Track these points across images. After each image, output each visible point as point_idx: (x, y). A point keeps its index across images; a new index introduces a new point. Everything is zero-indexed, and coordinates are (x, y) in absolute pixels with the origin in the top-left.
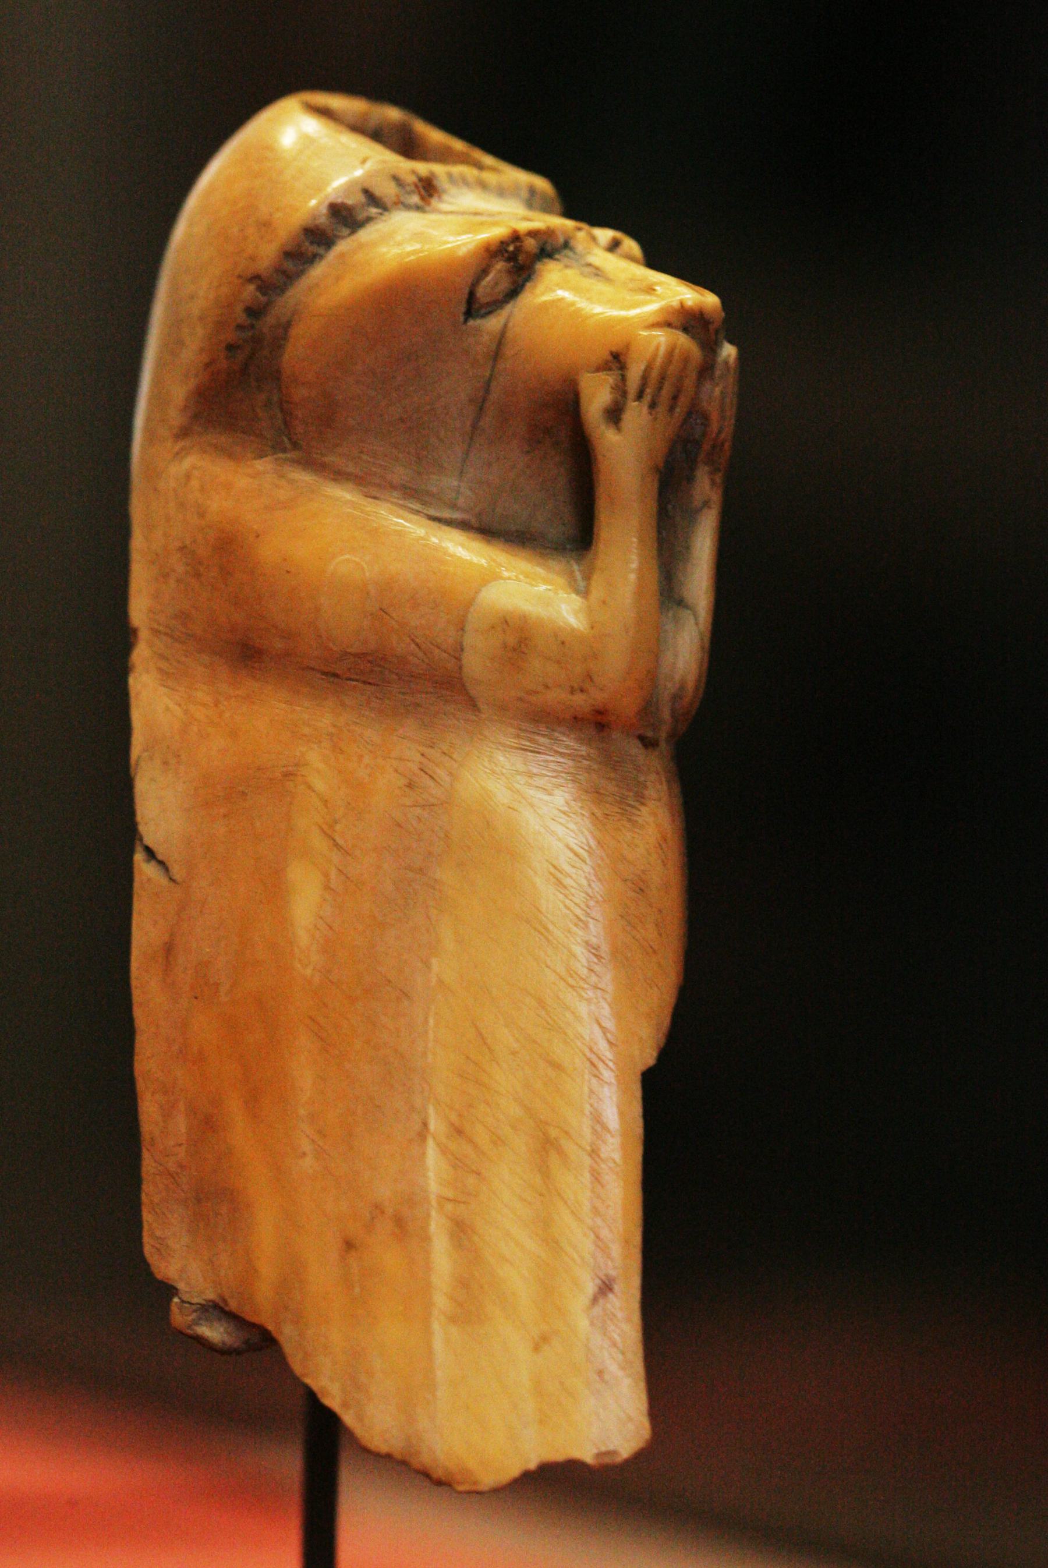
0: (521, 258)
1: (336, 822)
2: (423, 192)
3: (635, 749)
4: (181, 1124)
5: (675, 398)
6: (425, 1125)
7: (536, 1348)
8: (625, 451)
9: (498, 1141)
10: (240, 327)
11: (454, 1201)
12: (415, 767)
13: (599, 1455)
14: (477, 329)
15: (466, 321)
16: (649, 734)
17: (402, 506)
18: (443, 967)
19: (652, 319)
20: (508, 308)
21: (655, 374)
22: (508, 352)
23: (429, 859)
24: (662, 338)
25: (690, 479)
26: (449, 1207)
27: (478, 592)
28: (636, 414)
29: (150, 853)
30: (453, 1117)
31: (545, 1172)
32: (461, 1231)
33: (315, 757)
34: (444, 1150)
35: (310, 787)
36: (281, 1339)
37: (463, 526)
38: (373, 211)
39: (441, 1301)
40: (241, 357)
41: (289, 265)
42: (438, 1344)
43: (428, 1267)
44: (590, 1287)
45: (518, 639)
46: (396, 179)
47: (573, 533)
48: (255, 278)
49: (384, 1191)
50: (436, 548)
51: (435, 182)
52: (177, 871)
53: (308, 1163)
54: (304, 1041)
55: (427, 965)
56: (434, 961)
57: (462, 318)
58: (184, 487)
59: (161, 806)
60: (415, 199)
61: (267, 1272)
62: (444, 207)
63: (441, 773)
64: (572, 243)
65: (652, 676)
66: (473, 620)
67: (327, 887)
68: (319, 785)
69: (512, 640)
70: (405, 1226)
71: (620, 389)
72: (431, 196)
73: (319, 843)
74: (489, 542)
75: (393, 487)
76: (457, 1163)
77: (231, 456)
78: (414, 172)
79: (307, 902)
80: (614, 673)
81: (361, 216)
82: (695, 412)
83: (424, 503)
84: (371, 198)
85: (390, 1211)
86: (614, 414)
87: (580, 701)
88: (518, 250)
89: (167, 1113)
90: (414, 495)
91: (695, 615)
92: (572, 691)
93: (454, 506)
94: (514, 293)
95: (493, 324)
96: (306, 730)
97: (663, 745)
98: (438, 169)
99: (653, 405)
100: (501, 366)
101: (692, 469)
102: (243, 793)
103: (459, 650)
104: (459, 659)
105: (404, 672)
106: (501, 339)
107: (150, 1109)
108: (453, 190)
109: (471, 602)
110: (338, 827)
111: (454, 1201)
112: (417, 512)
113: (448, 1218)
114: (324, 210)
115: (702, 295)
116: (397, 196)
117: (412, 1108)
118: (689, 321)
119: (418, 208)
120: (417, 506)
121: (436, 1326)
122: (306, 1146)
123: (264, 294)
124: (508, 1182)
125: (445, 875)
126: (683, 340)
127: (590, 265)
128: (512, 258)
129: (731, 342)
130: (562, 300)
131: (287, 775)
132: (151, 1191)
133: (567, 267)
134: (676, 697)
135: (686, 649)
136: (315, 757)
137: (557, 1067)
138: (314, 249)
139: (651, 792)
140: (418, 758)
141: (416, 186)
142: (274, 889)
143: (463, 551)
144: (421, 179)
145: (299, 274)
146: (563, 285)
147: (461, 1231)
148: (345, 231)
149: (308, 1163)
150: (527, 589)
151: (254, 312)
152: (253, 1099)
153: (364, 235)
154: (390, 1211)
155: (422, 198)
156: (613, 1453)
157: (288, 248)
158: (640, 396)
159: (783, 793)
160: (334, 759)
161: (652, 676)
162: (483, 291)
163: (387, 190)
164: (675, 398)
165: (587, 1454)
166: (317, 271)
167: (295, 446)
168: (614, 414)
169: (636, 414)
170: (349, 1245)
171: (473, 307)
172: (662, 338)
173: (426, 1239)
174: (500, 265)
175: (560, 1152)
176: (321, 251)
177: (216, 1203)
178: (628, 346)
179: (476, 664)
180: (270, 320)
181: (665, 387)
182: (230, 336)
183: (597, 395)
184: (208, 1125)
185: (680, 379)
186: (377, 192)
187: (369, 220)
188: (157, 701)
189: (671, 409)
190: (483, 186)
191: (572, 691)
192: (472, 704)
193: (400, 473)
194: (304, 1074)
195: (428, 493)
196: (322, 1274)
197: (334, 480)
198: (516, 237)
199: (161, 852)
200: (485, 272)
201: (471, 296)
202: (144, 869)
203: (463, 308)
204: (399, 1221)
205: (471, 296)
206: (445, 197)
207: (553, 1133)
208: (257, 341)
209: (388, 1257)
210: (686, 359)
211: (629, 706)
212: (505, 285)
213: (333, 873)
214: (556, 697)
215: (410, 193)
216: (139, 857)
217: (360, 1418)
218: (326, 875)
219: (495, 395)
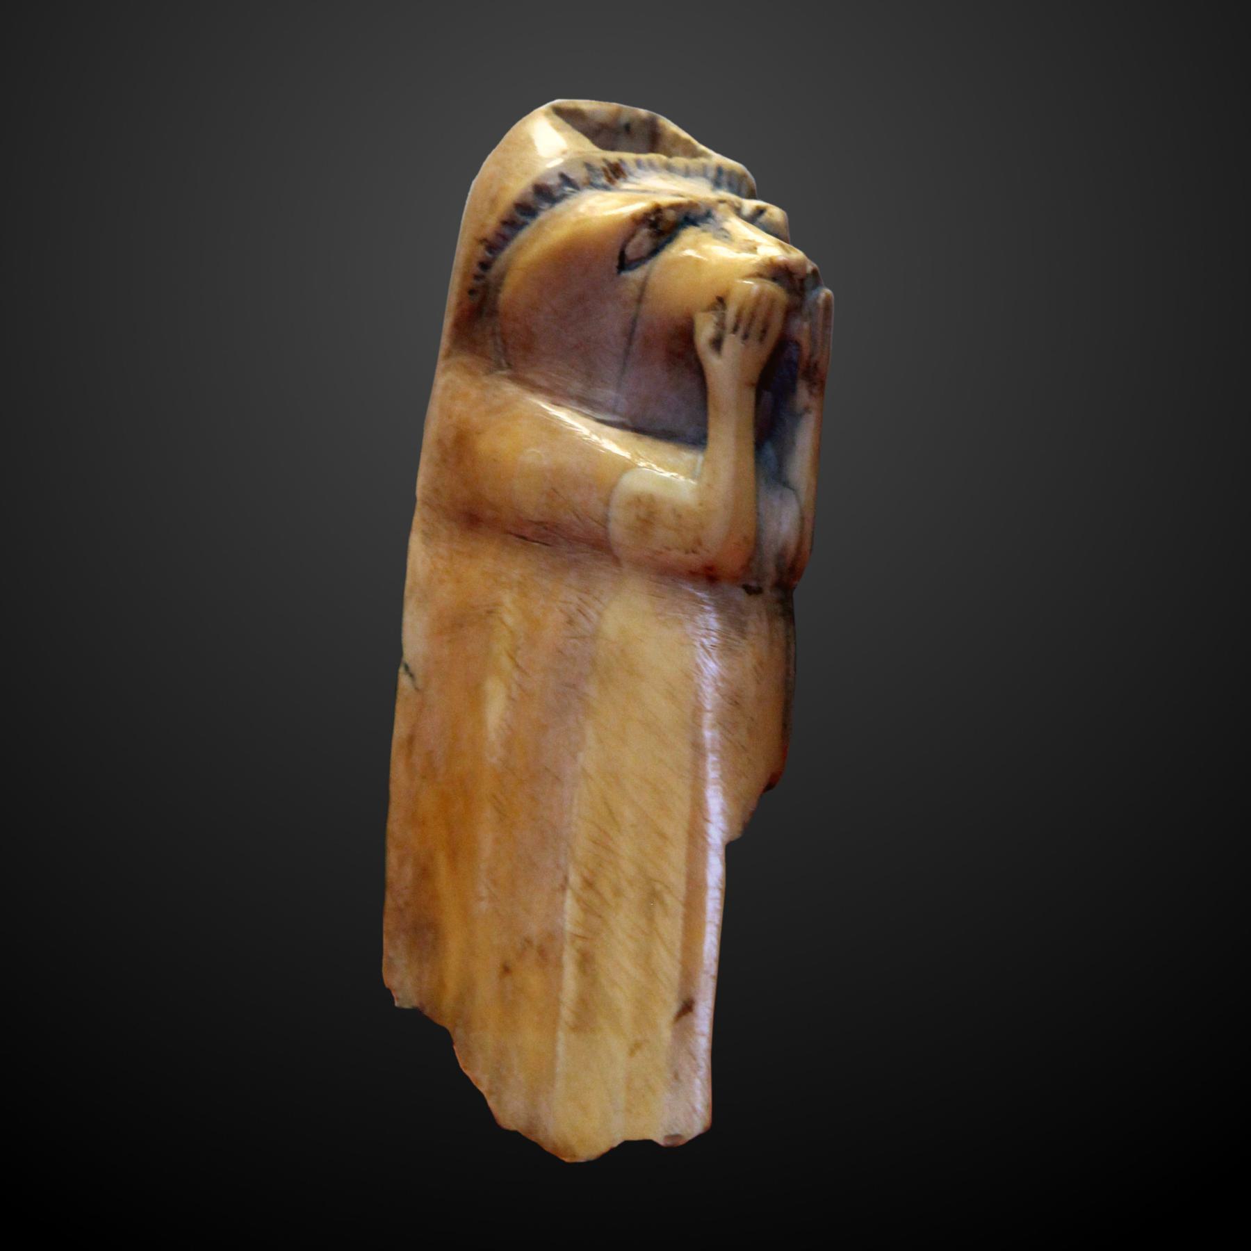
0: (661, 226)
1: (519, 648)
2: (611, 175)
3: (740, 596)
4: (409, 872)
5: (764, 332)
6: (566, 879)
7: (632, 1053)
8: (727, 369)
9: (618, 892)
10: (477, 277)
11: (583, 938)
12: (573, 608)
13: (668, 1137)
14: (625, 279)
15: (619, 273)
16: (753, 584)
17: (578, 412)
18: (589, 759)
19: (749, 270)
20: (647, 267)
21: (746, 313)
22: (648, 296)
23: (573, 681)
24: (753, 286)
25: (793, 391)
26: (579, 943)
27: (620, 476)
28: (732, 344)
29: (407, 668)
30: (586, 874)
31: (651, 920)
32: (586, 961)
33: (508, 599)
34: (579, 899)
35: (503, 623)
37: (621, 426)
38: (568, 189)
39: (566, 1014)
40: (477, 298)
41: (506, 231)
42: (561, 1049)
43: (560, 989)
44: (675, 1008)
45: (648, 512)
46: (588, 166)
47: (687, 432)
48: (483, 241)
49: (534, 929)
50: (594, 444)
51: (623, 167)
52: (420, 682)
53: (484, 906)
54: (488, 813)
55: (575, 757)
56: (581, 756)
57: (615, 271)
58: (457, 393)
59: (416, 633)
60: (604, 180)
61: (452, 986)
62: (626, 186)
63: (591, 613)
64: (714, 212)
65: (756, 542)
66: (618, 498)
67: (510, 698)
68: (509, 620)
69: (642, 514)
70: (545, 953)
71: (721, 325)
72: (618, 177)
73: (505, 662)
74: (639, 439)
75: (572, 397)
76: (587, 908)
77: (471, 373)
78: (605, 160)
79: (496, 710)
80: (717, 537)
81: (557, 194)
83: (594, 409)
84: (565, 179)
85: (536, 943)
86: (717, 343)
87: (695, 560)
88: (658, 219)
89: (402, 862)
90: (584, 403)
91: (797, 496)
92: (687, 552)
93: (614, 412)
94: (655, 251)
95: (636, 275)
96: (503, 579)
97: (767, 591)
98: (628, 157)
99: (745, 337)
100: (644, 306)
101: (794, 382)
102: (462, 623)
103: (604, 521)
104: (605, 527)
105: (566, 534)
106: (643, 286)
108: (640, 172)
109: (612, 487)
110: (519, 652)
111: (583, 938)
112: (586, 416)
113: (578, 951)
114: (530, 190)
115: (788, 252)
116: (588, 178)
117: (558, 867)
118: (779, 273)
119: (606, 188)
120: (588, 412)
121: (561, 1035)
122: (484, 892)
123: (490, 252)
124: (623, 921)
125: (592, 689)
126: (771, 287)
127: (723, 229)
128: (653, 225)
130: (690, 257)
131: (490, 612)
133: (704, 231)
136: (508, 599)
137: (663, 836)
138: (522, 218)
139: (751, 628)
140: (576, 600)
141: (605, 170)
142: (475, 696)
143: (612, 444)
144: (610, 165)
145: (514, 235)
146: (694, 246)
147: (586, 961)
148: (546, 205)
149: (484, 906)
150: (663, 475)
151: (485, 265)
152: (453, 856)
153: (559, 208)
154: (536, 943)
155: (610, 180)
157: (506, 218)
158: (735, 330)
160: (520, 598)
161: (756, 542)
162: (630, 252)
163: (578, 174)
164: (764, 332)
165: (659, 1137)
166: (524, 234)
167: (509, 366)
168: (717, 343)
169: (732, 344)
170: (506, 970)
171: (624, 263)
172: (753, 286)
173: (559, 965)
174: (645, 231)
175: (663, 903)
176: (528, 220)
177: (426, 935)
178: (728, 291)
179: (618, 531)
180: (494, 271)
183: (705, 331)
184: (425, 873)
185: (769, 313)
186: (572, 176)
187: (564, 196)
188: (421, 556)
189: (761, 340)
190: (669, 168)
191: (687, 552)
192: (617, 561)
193: (576, 387)
194: (487, 839)
195: (595, 402)
196: (486, 988)
197: (532, 392)
198: (658, 210)
199: (411, 665)
200: (633, 236)
201: (622, 255)
202: (404, 680)
203: (616, 263)
204: (542, 952)
205: (622, 255)
206: (630, 178)
207: (658, 887)
208: (486, 287)
209: (533, 981)
210: (773, 301)
211: (732, 562)
212: (647, 246)
213: (514, 687)
214: (676, 555)
215: (598, 176)
216: (402, 670)
218: (509, 688)
219: (638, 329)
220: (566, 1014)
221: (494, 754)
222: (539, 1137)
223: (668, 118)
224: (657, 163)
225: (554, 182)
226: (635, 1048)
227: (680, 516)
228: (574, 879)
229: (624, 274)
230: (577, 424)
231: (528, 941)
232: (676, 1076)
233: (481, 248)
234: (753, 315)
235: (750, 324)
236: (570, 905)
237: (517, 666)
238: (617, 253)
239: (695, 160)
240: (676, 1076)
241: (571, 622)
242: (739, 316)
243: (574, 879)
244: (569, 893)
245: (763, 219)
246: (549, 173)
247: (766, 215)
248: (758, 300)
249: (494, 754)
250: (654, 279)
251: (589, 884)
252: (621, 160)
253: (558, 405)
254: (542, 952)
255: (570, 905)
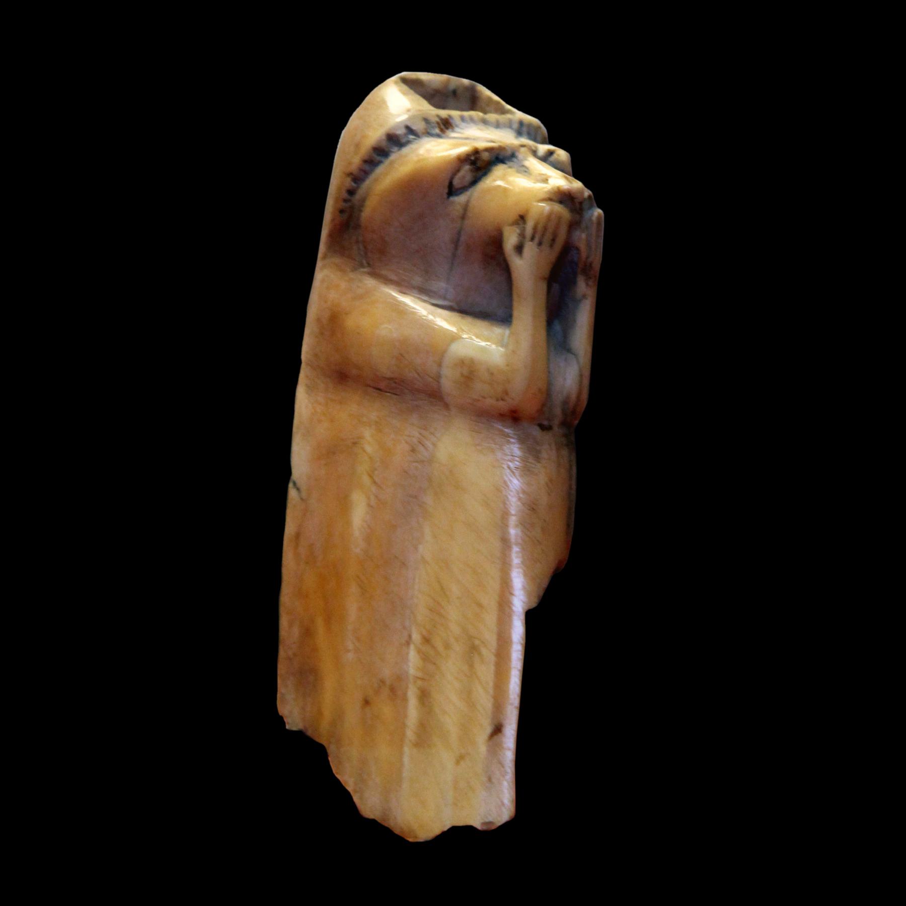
0: (479, 164)
1: (376, 469)
2: (442, 127)
3: (536, 431)
4: (296, 631)
5: (553, 240)
6: (410, 636)
7: (458, 762)
8: (526, 267)
9: (447, 646)
10: (345, 201)
11: (422, 679)
12: (415, 440)
13: (484, 824)
14: (453, 202)
15: (448, 197)
16: (546, 423)
17: (419, 298)
18: (426, 549)
19: (543, 196)
20: (468, 193)
21: (540, 227)
22: (469, 214)
23: (415, 493)
24: (546, 207)
25: (574, 283)
26: (419, 683)
27: (449, 345)
28: (530, 249)
29: (295, 484)
30: (424, 633)
31: (471, 666)
32: (424, 696)
33: (368, 434)
34: (419, 651)
35: (364, 451)
36: (329, 751)
37: (450, 308)
38: (411, 137)
39: (410, 734)
40: (345, 216)
41: (367, 167)
42: (406, 760)
43: (406, 716)
44: (489, 730)
45: (469, 371)
46: (426, 120)
47: (498, 313)
48: (350, 174)
49: (387, 672)
50: (430, 321)
51: (451, 121)
52: (304, 494)
53: (350, 656)
54: (354, 589)
55: (416, 548)
56: (421, 548)
57: (445, 196)
60: (437, 131)
61: (327, 714)
62: (453, 135)
63: (428, 444)
64: (517, 154)
65: (548, 393)
66: (448, 361)
67: (369, 505)
68: (369, 449)
69: (465, 372)
70: (394, 690)
71: (522, 235)
72: (447, 128)
73: (366, 480)
74: (463, 318)
75: (414, 288)
76: (425, 658)
77: (341, 270)
78: (438, 116)
79: (359, 514)
80: (519, 389)
81: (404, 140)
82: (568, 248)
83: (430, 296)
84: (409, 130)
85: (388, 683)
86: (519, 249)
87: (503, 406)
88: (477, 159)
89: (291, 625)
90: (423, 292)
91: (577, 359)
92: (497, 400)
93: (445, 298)
94: (475, 182)
95: (461, 199)
96: (365, 419)
97: (556, 428)
98: (455, 114)
99: (540, 244)
100: (466, 222)
101: (575, 277)
102: (334, 451)
103: (438, 378)
104: (438, 382)
105: (410, 386)
106: (466, 207)
107: (284, 621)
108: (463, 125)
109: (443, 353)
110: (376, 472)
111: (422, 679)
112: (425, 301)
113: (419, 689)
114: (384, 138)
116: (426, 129)
117: (404, 628)
118: (564, 198)
119: (439, 136)
120: (426, 298)
121: (406, 749)
122: (351, 646)
123: (355, 182)
124: (451, 667)
125: (429, 499)
126: (558, 208)
127: (523, 166)
128: (473, 163)
129: (599, 207)
130: (500, 186)
131: (355, 443)
132: (282, 668)
133: (510, 167)
134: (565, 402)
135: (572, 376)
136: (368, 434)
137: (480, 605)
138: (378, 158)
139: (544, 455)
140: (417, 434)
141: (438, 123)
142: (344, 504)
143: (444, 321)
144: (442, 119)
145: (372, 171)
146: (503, 178)
147: (424, 696)
148: (396, 149)
149: (350, 656)
150: (480, 344)
151: (351, 192)
152: (328, 620)
153: (405, 150)
154: (388, 683)
155: (442, 130)
156: (491, 823)
157: (366, 158)
158: (532, 239)
159: (619, 457)
161: (548, 393)
162: (456, 182)
163: (419, 126)
164: (553, 240)
165: (477, 824)
166: (380, 170)
167: (369, 265)
168: (519, 249)
169: (530, 249)
170: (367, 702)
171: (452, 191)
172: (546, 207)
173: (405, 699)
174: (467, 167)
175: (480, 654)
176: (383, 159)
177: (309, 677)
178: (527, 211)
179: (447, 384)
180: (357, 197)
181: (544, 233)
183: (511, 240)
184: (308, 632)
185: (557, 227)
186: (414, 128)
187: (409, 142)
188: (306, 402)
189: (551, 246)
190: (485, 122)
191: (497, 400)
192: (447, 406)
193: (417, 280)
194: (352, 608)
195: (431, 291)
196: (352, 716)
197: (386, 284)
198: (476, 152)
200: (458, 171)
201: (451, 185)
203: (446, 191)
204: (393, 690)
205: (451, 185)
206: (457, 129)
207: (477, 642)
208: (352, 208)
209: (386, 710)
210: (560, 218)
211: (530, 407)
212: (469, 178)
213: (372, 497)
214: (489, 402)
215: (433, 127)
216: (291, 485)
217: (361, 798)
218: (369, 498)
219: (462, 239)
220: (410, 734)
221: (358, 546)
222: (391, 824)
223: (484, 85)
224: (476, 118)
225: (401, 131)
226: (460, 759)
227: (492, 374)
228: (416, 637)
229: (452, 199)
230: (418, 307)
231: (383, 682)
232: (490, 779)
233: (349, 180)
234: (545, 228)
235: (543, 235)
236: (413, 655)
237: (375, 482)
238: (447, 183)
239: (503, 116)
240: (490, 779)
241: (413, 450)
242: (535, 229)
243: (416, 637)
244: (412, 647)
246: (397, 126)
248: (549, 217)
249: (358, 546)
250: (473, 202)
251: (427, 640)
252: (450, 116)
253: (404, 293)
254: (393, 690)
255: (413, 655)
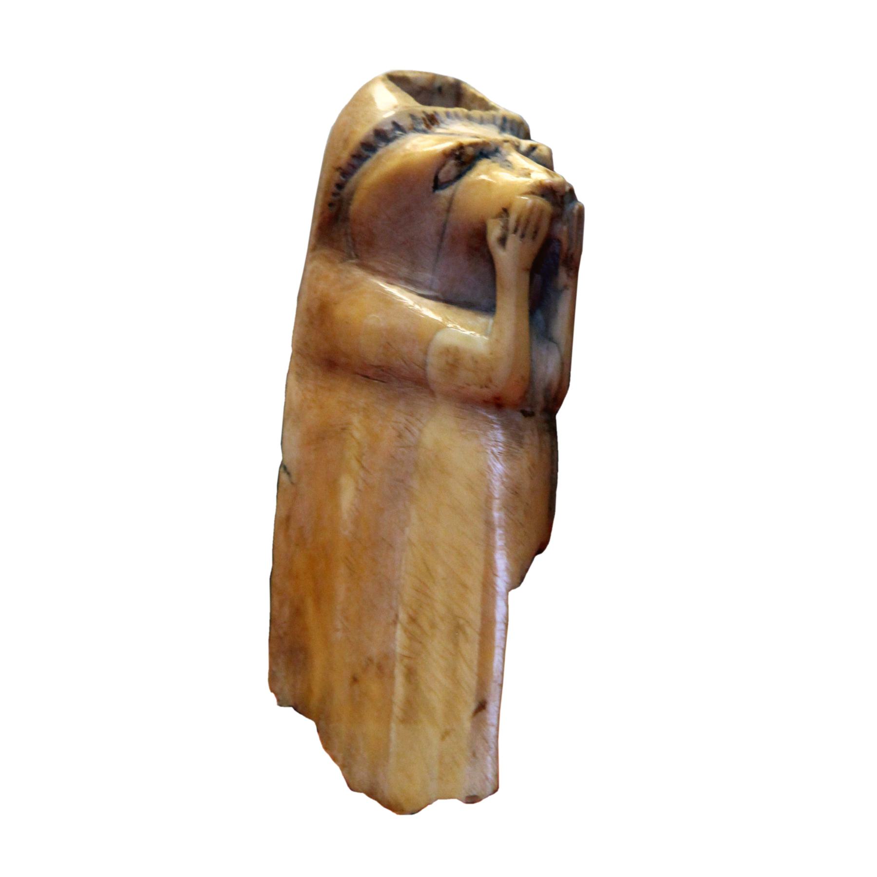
0: (464, 159)
1: (364, 454)
2: (428, 123)
3: (519, 418)
5: (536, 232)
6: (397, 616)
7: (443, 738)
9: (433, 626)
10: (334, 194)
11: (409, 657)
12: (402, 426)
14: (438, 196)
15: (434, 191)
16: (528, 409)
17: (405, 289)
18: (413, 532)
19: (525, 190)
20: (453, 187)
21: (523, 220)
22: (454, 207)
24: (528, 200)
25: (556, 274)
26: (406, 661)
27: (434, 334)
28: (513, 241)
30: (411, 612)
31: (456, 645)
32: (411, 674)
33: (356, 420)
34: (406, 630)
35: (353, 436)
37: (435, 299)
38: (398, 132)
39: (397, 711)
40: (334, 209)
41: (355, 162)
42: (393, 735)
43: (393, 693)
44: (473, 706)
45: (454, 359)
46: (412, 116)
47: (482, 303)
48: (339, 169)
49: (374, 651)
50: (416, 311)
51: (437, 117)
52: (294, 478)
53: (339, 635)
54: (342, 570)
55: (403, 531)
56: (407, 530)
57: (431, 190)
60: (423, 127)
61: (317, 691)
62: (439, 130)
63: (415, 430)
64: (500, 149)
66: (433, 349)
67: (357, 489)
68: (357, 435)
69: (450, 360)
70: (382, 668)
71: (505, 228)
72: (433, 124)
73: (354, 464)
75: (401, 278)
76: (411, 637)
77: (330, 261)
78: (424, 112)
79: (348, 498)
81: (391, 136)
83: (416, 287)
84: (396, 126)
85: (376, 661)
86: (503, 241)
87: (487, 393)
88: (461, 154)
90: (410, 282)
91: (559, 348)
92: (481, 387)
93: (430, 289)
94: (459, 176)
95: (446, 193)
96: (353, 406)
97: (538, 415)
98: (440, 110)
99: (523, 236)
100: (451, 215)
101: (557, 268)
103: (424, 366)
104: (424, 370)
106: (451, 201)
108: (448, 121)
109: (429, 342)
110: (364, 457)
111: (409, 657)
112: (411, 291)
113: (405, 667)
114: (372, 133)
116: (412, 125)
117: (391, 607)
119: (425, 132)
120: (412, 289)
121: (393, 725)
122: (339, 626)
123: (344, 177)
124: (437, 646)
125: (415, 483)
126: (540, 201)
127: (507, 161)
128: (458, 158)
130: (484, 180)
131: (343, 429)
133: (494, 162)
136: (356, 420)
137: (465, 586)
138: (366, 153)
139: (527, 440)
140: (404, 421)
141: (424, 119)
142: (333, 488)
143: (429, 311)
144: (427, 115)
145: (360, 165)
146: (487, 172)
147: (411, 674)
148: (383, 144)
149: (339, 635)
151: (340, 186)
152: (318, 600)
153: (392, 145)
154: (376, 661)
155: (428, 126)
157: (354, 153)
158: (515, 231)
161: (530, 380)
162: (442, 176)
163: (405, 122)
164: (536, 232)
166: (367, 164)
167: (357, 256)
168: (503, 241)
169: (513, 241)
170: (355, 680)
171: (437, 185)
172: (528, 200)
173: (392, 677)
174: (452, 162)
175: (464, 633)
176: (370, 154)
178: (510, 204)
179: (433, 372)
180: (346, 190)
182: (331, 198)
183: (494, 232)
185: (539, 219)
186: (401, 124)
187: (396, 138)
189: (534, 238)
190: (469, 118)
191: (481, 387)
192: (432, 393)
193: (404, 271)
194: (341, 588)
195: (417, 282)
197: (373, 275)
198: (461, 147)
200: (443, 165)
201: (436, 179)
203: (432, 184)
204: (380, 667)
205: (436, 179)
206: (442, 125)
207: (462, 622)
208: (341, 201)
209: (374, 687)
210: (542, 211)
211: (513, 394)
212: (454, 172)
213: (360, 482)
214: (474, 389)
215: (419, 123)
218: (357, 482)
219: (448, 231)
220: (397, 711)
221: (346, 529)
224: (461, 114)
226: (445, 735)
227: (476, 362)
228: (403, 616)
229: (437, 192)
230: (404, 297)
231: (370, 660)
232: (474, 755)
233: (338, 174)
234: (528, 221)
235: (526, 227)
236: (399, 634)
237: (363, 467)
238: (432, 178)
240: (474, 755)
241: (400, 436)
242: (518, 222)
243: (403, 616)
244: (399, 626)
245: (535, 153)
246: (385, 122)
247: (537, 151)
248: (531, 210)
249: (346, 529)
250: (458, 196)
251: (413, 620)
252: (435, 112)
254: (380, 667)
255: (399, 634)
